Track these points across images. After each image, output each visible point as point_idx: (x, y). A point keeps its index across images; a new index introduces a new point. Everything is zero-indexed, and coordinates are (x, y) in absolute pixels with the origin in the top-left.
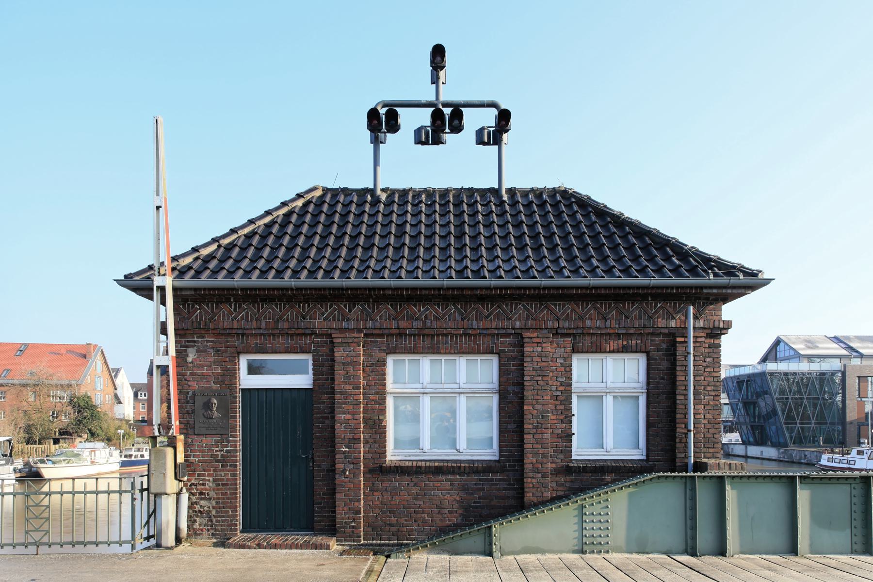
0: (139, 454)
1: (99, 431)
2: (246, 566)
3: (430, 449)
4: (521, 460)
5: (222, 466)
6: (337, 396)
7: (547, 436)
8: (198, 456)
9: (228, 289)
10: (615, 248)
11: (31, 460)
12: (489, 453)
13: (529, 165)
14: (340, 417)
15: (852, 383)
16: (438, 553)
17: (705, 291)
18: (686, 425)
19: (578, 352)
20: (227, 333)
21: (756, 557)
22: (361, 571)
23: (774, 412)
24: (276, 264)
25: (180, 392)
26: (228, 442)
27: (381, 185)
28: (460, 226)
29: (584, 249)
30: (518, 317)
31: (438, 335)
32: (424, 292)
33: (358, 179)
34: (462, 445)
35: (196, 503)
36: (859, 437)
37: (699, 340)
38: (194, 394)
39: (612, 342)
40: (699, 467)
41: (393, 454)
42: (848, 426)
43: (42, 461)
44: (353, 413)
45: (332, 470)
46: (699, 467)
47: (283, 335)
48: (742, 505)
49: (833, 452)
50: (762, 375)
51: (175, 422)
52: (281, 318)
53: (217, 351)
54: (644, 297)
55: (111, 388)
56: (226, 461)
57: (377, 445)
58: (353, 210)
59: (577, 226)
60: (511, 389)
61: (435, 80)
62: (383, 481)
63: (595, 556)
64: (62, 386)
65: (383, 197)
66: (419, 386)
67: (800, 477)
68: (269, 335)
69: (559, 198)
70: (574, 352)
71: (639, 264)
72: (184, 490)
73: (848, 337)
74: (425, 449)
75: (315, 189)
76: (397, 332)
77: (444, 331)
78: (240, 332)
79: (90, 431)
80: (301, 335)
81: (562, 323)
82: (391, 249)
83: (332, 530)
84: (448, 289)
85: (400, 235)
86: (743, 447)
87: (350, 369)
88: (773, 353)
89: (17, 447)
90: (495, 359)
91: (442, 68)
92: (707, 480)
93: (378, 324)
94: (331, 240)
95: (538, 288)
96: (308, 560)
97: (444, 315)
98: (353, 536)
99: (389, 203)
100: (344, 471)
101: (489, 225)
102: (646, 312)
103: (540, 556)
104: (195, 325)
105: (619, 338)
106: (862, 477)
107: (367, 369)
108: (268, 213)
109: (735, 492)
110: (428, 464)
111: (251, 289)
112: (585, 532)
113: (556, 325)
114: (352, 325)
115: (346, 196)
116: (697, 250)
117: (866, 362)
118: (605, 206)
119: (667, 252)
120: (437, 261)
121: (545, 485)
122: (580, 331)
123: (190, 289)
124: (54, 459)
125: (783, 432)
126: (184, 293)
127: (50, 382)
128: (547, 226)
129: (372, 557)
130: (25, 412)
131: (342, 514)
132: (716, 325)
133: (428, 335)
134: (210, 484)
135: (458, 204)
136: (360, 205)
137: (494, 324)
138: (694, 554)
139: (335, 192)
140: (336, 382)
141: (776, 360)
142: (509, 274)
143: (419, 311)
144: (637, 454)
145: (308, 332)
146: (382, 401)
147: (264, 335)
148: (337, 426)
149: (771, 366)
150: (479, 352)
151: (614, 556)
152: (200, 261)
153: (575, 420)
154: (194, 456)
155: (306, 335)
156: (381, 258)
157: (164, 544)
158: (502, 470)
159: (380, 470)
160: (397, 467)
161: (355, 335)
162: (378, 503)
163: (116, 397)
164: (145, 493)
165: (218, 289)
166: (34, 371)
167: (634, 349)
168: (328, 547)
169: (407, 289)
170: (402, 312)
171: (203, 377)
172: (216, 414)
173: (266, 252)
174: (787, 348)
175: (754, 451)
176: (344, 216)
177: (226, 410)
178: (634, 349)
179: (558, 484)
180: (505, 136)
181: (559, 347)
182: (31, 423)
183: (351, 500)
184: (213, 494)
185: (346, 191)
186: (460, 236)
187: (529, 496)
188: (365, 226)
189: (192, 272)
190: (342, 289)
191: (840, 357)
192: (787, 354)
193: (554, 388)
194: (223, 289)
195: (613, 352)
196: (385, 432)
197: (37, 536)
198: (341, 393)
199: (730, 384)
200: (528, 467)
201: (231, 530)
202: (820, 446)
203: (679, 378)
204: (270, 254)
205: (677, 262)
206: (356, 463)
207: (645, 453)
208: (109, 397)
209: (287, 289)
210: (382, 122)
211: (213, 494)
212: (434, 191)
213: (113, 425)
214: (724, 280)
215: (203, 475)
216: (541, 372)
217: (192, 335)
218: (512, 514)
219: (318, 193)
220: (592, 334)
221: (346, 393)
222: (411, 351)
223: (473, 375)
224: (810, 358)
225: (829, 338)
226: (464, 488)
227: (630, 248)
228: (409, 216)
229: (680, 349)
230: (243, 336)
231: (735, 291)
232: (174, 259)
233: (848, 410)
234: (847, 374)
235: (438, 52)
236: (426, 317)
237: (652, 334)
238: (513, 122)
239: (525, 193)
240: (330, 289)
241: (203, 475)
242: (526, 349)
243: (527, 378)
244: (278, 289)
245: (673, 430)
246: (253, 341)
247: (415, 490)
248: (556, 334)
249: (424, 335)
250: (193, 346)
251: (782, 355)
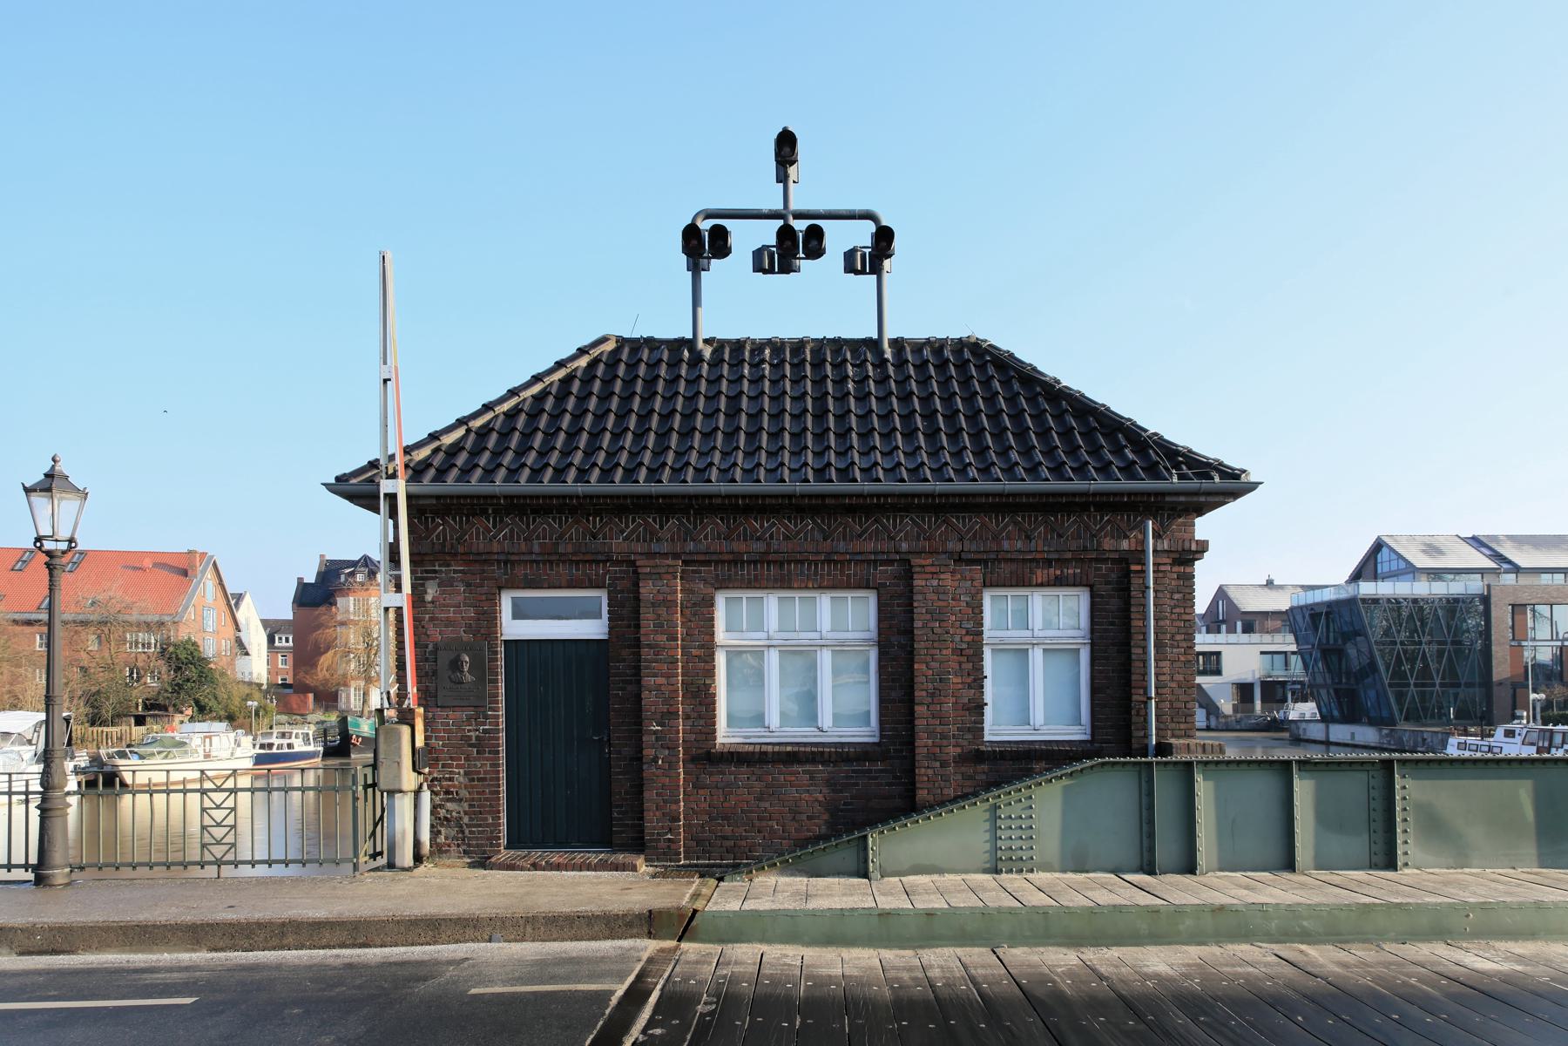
0: (285, 742)
1: (213, 703)
2: (522, 891)
3: (778, 723)
4: (910, 743)
6: (644, 651)
7: (949, 706)
8: (442, 738)
9: (486, 497)
10: (1044, 434)
11: (103, 752)
12: (864, 732)
13: (923, 305)
14: (649, 681)
15: (1501, 616)
16: (792, 875)
17: (1168, 499)
18: (1146, 689)
19: (991, 586)
20: (480, 560)
21: (1238, 874)
22: (684, 895)
23: (1372, 666)
24: (554, 458)
25: (417, 645)
26: (486, 717)
27: (704, 333)
28: (821, 399)
29: (999, 435)
30: (904, 534)
31: (789, 562)
32: (768, 501)
33: (667, 321)
34: (826, 720)
35: (441, 806)
36: (1514, 707)
37: (1162, 568)
38: (436, 648)
39: (1039, 572)
40: (1163, 749)
41: (725, 735)
42: (1495, 689)
43: (122, 755)
44: (668, 676)
45: (638, 758)
46: (1163, 749)
47: (564, 562)
48: (1221, 803)
49: (1466, 734)
50: (1352, 602)
51: (412, 689)
52: (561, 537)
53: (468, 585)
54: (1084, 507)
55: (231, 628)
56: (483, 745)
57: (702, 722)
58: (693, 460)
59: (991, 399)
60: (894, 639)
61: (782, 178)
62: (711, 774)
63: (1014, 876)
64: (148, 624)
65: (707, 352)
66: (763, 635)
67: (1299, 762)
68: (544, 562)
69: (967, 354)
70: (985, 586)
71: (1077, 459)
72: (425, 786)
73: (1495, 538)
74: (772, 728)
75: (604, 340)
76: (731, 557)
77: (798, 557)
78: (502, 557)
79: (197, 702)
80: (590, 562)
81: (966, 543)
82: (720, 436)
83: (638, 844)
84: (803, 496)
85: (733, 414)
86: (1322, 726)
87: (663, 611)
88: (1371, 565)
89: (77, 730)
90: (871, 598)
91: (793, 163)
92: (1170, 767)
93: (702, 547)
94: (633, 421)
95: (932, 495)
96: (607, 883)
97: (798, 533)
98: (669, 853)
99: (716, 362)
100: (655, 760)
101: (863, 398)
102: (1087, 528)
103: (935, 877)
104: (437, 548)
105: (1050, 566)
106: (1383, 761)
107: (687, 612)
108: (537, 379)
109: (1211, 784)
110: (777, 749)
111: (518, 497)
112: (999, 843)
113: (959, 547)
114: (665, 547)
115: (651, 350)
116: (1161, 438)
117: (1524, 580)
118: (1034, 369)
119: (1117, 441)
120: (787, 454)
121: (946, 779)
122: (993, 556)
123: (431, 497)
124: (141, 750)
125: (1388, 699)
126: (421, 502)
127: (127, 618)
128: (948, 399)
129: (697, 881)
130: (84, 670)
131: (652, 822)
132: (1187, 546)
133: (775, 562)
134: (460, 779)
135: (818, 364)
136: (674, 364)
137: (870, 546)
138: (1152, 873)
139: (636, 345)
140: (643, 631)
141: (1375, 577)
142: (891, 475)
143: (762, 526)
144: (1076, 732)
145: (600, 557)
146: (709, 658)
147: (537, 562)
148: (645, 694)
149: (1367, 588)
150: (848, 586)
151: (1040, 877)
152: (441, 455)
153: (988, 683)
154: (437, 738)
155: (598, 562)
156: (705, 450)
157: (398, 863)
158: (884, 756)
159: (708, 758)
160: (731, 754)
161: (670, 562)
162: (705, 806)
163: (239, 643)
164: (370, 790)
165: (472, 497)
166: (100, 597)
167: (1071, 580)
168: (634, 868)
169: (744, 497)
170: (737, 528)
171: (449, 623)
172: (469, 678)
173: (538, 440)
174: (1394, 556)
175: (1340, 732)
176: (651, 382)
177: (483, 670)
178: (1071, 580)
179: (966, 777)
180: (886, 263)
181: (964, 578)
182: (94, 689)
183: (665, 802)
184: (464, 793)
185: (651, 343)
186: (820, 416)
187: (922, 794)
188: (680, 399)
189: (432, 472)
190: (650, 497)
191: (1482, 572)
192: (1394, 567)
193: (957, 638)
194: (478, 497)
195: (1042, 585)
196: (714, 703)
197: (218, 851)
198: (649, 646)
199: (1299, 618)
200: (921, 752)
201: (492, 845)
202: (1449, 722)
203: (1134, 623)
204: (544, 442)
205: (1131, 456)
206: (673, 748)
207: (1089, 731)
208: (226, 644)
209: (571, 497)
210: (703, 244)
211: (464, 793)
212: (783, 342)
213: (238, 692)
214: (1195, 484)
215: (451, 766)
216: (938, 615)
217: (432, 563)
218: (896, 819)
219: (610, 346)
220: (1012, 560)
221: (657, 646)
222: (751, 584)
223: (841, 619)
224: (1436, 574)
225: (1464, 539)
226: (831, 783)
227: (1066, 434)
228: (746, 383)
229: (1135, 581)
230: (506, 563)
231: (1210, 499)
232: (408, 450)
233: (1494, 662)
234: (1493, 600)
235: (786, 145)
236: (771, 537)
237: (1097, 560)
238: (896, 244)
239: (918, 347)
240: (632, 497)
241: (451, 766)
242: (916, 583)
243: (917, 624)
244: (558, 497)
245: (1128, 697)
246: (520, 571)
247: (758, 786)
248: (959, 560)
249: (769, 563)
251: (1386, 569)
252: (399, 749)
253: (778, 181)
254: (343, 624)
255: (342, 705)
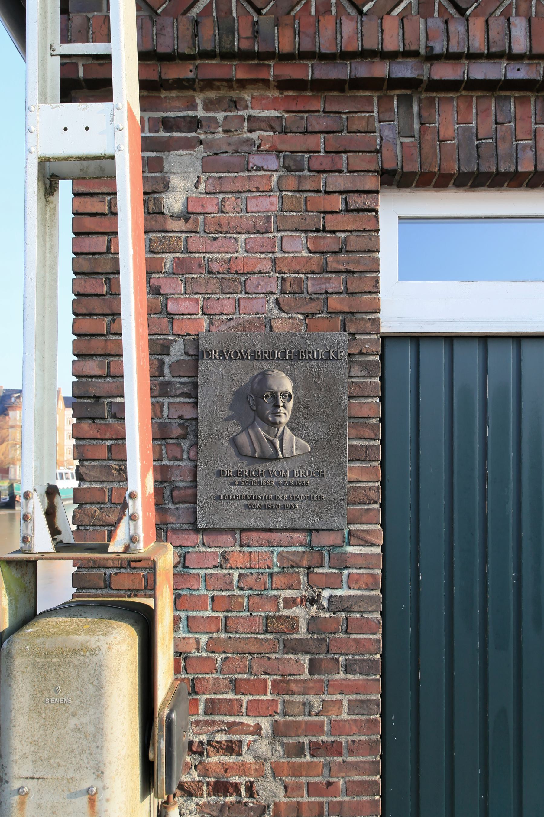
5: (314, 667)
38: (196, 355)
171: (235, 278)
172: (293, 444)
241: (232, 708)
250: (189, 145)
252: (96, 735)
253: (94, 395)
254: (12, 427)
255: (11, 475)
